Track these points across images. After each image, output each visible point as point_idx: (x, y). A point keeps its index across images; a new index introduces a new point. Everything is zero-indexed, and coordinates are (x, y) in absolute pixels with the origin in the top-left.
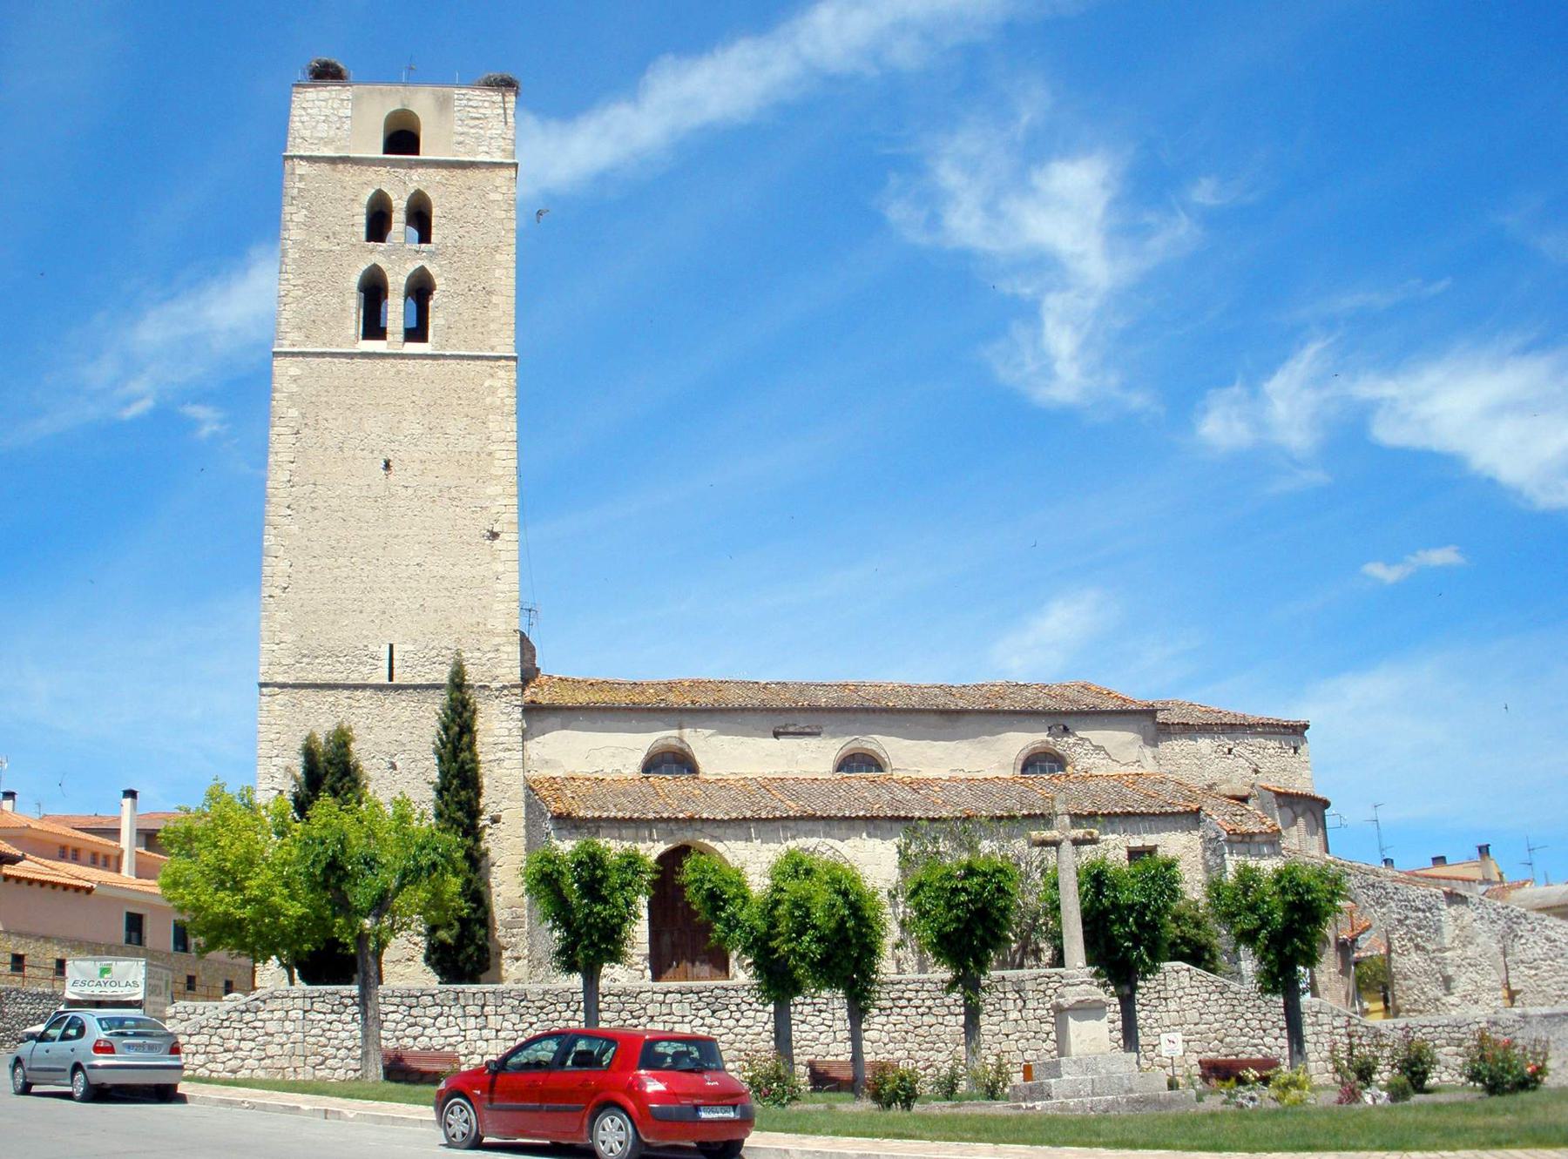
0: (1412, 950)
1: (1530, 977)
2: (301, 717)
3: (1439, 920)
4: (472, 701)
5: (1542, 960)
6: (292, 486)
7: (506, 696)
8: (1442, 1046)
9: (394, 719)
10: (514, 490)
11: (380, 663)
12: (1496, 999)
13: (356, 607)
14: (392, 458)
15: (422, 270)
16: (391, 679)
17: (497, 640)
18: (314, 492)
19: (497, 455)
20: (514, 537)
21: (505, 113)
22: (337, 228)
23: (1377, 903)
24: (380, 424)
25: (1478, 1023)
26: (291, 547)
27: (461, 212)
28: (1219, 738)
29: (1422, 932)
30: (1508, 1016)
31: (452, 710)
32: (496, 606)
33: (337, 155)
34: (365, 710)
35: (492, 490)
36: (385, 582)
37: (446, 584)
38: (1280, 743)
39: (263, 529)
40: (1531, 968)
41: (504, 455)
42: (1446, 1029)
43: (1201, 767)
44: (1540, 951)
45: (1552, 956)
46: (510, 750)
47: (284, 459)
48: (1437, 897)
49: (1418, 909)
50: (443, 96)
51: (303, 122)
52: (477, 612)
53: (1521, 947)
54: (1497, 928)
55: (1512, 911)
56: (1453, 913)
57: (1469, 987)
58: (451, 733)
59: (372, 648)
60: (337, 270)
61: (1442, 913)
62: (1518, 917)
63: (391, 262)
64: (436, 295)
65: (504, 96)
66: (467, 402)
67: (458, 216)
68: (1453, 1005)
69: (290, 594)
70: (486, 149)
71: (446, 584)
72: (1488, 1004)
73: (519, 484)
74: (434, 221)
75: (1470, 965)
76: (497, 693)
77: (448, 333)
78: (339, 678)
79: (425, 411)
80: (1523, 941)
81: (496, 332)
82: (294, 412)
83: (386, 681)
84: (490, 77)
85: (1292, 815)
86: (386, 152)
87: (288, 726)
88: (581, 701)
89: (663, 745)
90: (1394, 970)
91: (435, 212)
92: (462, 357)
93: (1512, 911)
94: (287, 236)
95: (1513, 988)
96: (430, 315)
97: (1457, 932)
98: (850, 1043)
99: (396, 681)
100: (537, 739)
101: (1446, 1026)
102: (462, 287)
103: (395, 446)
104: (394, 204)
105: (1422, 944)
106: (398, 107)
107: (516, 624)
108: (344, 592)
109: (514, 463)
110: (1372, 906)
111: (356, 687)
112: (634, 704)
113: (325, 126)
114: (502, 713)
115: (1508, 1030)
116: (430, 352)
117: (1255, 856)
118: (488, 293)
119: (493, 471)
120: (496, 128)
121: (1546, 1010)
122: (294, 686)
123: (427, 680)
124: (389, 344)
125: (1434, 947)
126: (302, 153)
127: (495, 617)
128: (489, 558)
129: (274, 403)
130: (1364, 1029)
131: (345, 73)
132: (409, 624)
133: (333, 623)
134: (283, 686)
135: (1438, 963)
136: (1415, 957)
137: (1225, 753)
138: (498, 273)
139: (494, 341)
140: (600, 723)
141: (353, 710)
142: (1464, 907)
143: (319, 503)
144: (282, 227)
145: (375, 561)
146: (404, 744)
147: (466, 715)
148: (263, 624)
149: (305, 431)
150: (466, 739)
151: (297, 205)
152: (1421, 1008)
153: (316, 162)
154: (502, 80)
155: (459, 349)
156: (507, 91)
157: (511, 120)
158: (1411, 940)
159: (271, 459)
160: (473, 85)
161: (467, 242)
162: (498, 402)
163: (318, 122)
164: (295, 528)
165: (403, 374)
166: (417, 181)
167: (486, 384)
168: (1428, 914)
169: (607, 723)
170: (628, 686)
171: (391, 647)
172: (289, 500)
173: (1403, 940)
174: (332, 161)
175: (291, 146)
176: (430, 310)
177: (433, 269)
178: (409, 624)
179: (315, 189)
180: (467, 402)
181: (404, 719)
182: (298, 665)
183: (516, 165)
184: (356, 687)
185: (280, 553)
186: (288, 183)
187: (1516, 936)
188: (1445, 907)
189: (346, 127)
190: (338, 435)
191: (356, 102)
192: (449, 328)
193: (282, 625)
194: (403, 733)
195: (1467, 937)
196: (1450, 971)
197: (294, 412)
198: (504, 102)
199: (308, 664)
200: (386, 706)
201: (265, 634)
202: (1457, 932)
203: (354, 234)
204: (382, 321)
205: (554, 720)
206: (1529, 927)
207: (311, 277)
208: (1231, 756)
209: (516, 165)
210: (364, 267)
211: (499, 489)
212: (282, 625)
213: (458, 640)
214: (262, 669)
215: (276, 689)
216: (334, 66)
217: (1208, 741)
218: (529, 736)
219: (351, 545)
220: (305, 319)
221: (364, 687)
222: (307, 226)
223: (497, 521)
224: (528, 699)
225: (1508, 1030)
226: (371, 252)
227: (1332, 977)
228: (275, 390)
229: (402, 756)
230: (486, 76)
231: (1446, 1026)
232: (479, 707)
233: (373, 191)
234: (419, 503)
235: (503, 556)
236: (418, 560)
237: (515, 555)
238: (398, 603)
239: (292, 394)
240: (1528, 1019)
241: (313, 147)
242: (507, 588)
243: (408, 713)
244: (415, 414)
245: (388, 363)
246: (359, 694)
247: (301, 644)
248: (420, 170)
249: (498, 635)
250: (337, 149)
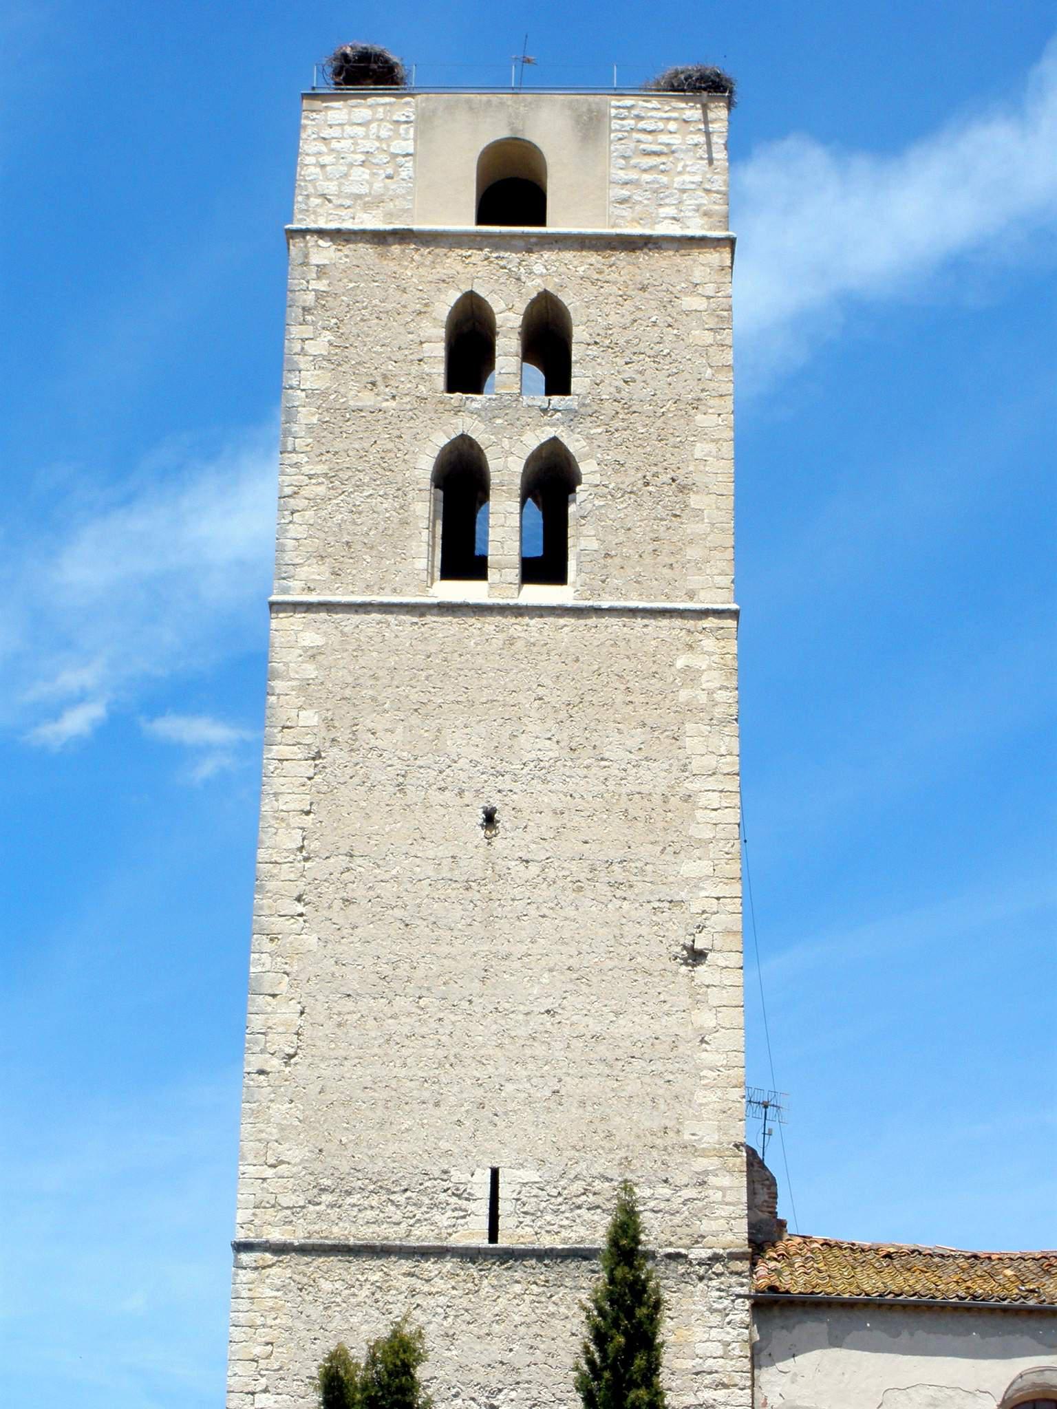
2: (315, 1312)
4: (652, 1284)
6: (306, 859)
7: (719, 1275)
9: (499, 1318)
10: (735, 868)
11: (471, 1206)
13: (426, 1095)
14: (498, 805)
15: (555, 441)
16: (493, 1237)
17: (701, 1164)
18: (348, 870)
19: (703, 800)
20: (736, 959)
21: (709, 143)
22: (390, 366)
24: (475, 740)
26: (303, 976)
27: (629, 334)
31: (613, 1302)
32: (701, 1096)
33: (389, 227)
34: (442, 1300)
35: (691, 868)
36: (484, 1046)
37: (602, 1050)
39: (249, 942)
41: (714, 800)
46: (725, 1386)
47: (291, 806)
50: (590, 111)
51: (323, 166)
52: (663, 1107)
58: (610, 1348)
59: (456, 1176)
60: (390, 446)
63: (496, 431)
64: (582, 492)
65: (705, 108)
66: (642, 699)
67: (622, 342)
69: (300, 1068)
70: (671, 211)
71: (602, 1050)
73: (744, 857)
74: (576, 352)
76: (702, 1271)
77: (605, 566)
78: (393, 1235)
79: (563, 715)
81: (699, 566)
82: (310, 718)
83: (484, 1243)
84: (676, 74)
86: (481, 220)
87: (289, 1329)
88: (867, 1288)
89: (1034, 1385)
91: (579, 334)
92: (633, 612)
94: (294, 383)
96: (570, 531)
98: (733, 497)
99: (503, 1242)
100: (781, 1365)
102: (631, 478)
103: (505, 783)
104: (499, 319)
106: (504, 133)
107: (739, 1133)
108: (405, 1065)
109: (734, 816)
111: (424, 1253)
112: (974, 1298)
113: (364, 173)
114: (712, 1311)
116: (570, 603)
118: (683, 489)
119: (693, 831)
120: (692, 170)
122: (303, 1250)
123: (564, 1241)
124: (491, 587)
126: (322, 224)
127: (699, 1118)
128: (685, 1001)
129: (273, 699)
131: (401, 72)
132: (531, 1129)
133: (382, 1124)
134: (281, 1249)
138: (700, 450)
139: (694, 581)
140: (905, 1335)
141: (418, 1300)
143: (357, 891)
144: (286, 367)
145: (465, 1004)
146: (516, 1370)
147: (641, 1312)
148: (246, 1129)
149: (332, 754)
150: (640, 1362)
151: (313, 323)
153: (348, 241)
154: (702, 78)
155: (625, 596)
156: (713, 99)
157: (720, 155)
159: (267, 806)
160: (645, 91)
161: (639, 391)
162: (703, 698)
163: (351, 165)
164: (311, 940)
165: (520, 644)
166: (541, 275)
167: (680, 663)
169: (920, 1335)
170: (961, 1262)
171: (495, 1173)
172: (301, 886)
174: (379, 238)
175: (302, 211)
176: (571, 522)
177: (574, 445)
178: (531, 1129)
179: (348, 292)
180: (642, 699)
181: (517, 1319)
182: (311, 1208)
183: (731, 242)
184: (424, 1253)
185: (283, 987)
186: (295, 282)
189: (404, 174)
190: (395, 761)
191: (423, 123)
192: (607, 555)
193: (282, 1129)
194: (516, 1347)
197: (310, 718)
198: (706, 122)
199: (332, 1206)
200: (483, 1293)
201: (249, 1146)
203: (424, 378)
204: (478, 545)
205: (813, 1326)
207: (345, 461)
209: (731, 242)
210: (442, 440)
211: (704, 867)
212: (282, 1129)
213: (626, 1162)
214: (242, 1216)
215: (268, 1256)
216: (379, 57)
218: (763, 1357)
219: (420, 973)
220: (331, 539)
221: (440, 1253)
222: (332, 362)
223: (701, 928)
224: (763, 1283)
226: (457, 411)
228: (275, 675)
229: (513, 1395)
230: (670, 70)
232: (666, 1296)
233: (459, 295)
234: (550, 893)
235: (714, 997)
236: (548, 1004)
237: (737, 996)
238: (509, 1087)
239: (307, 683)
241: (343, 212)
242: (720, 1060)
243: (525, 1308)
244: (543, 720)
245: (491, 623)
246: (430, 1267)
247: (318, 1166)
248: (547, 255)
249: (704, 1153)
250: (389, 215)
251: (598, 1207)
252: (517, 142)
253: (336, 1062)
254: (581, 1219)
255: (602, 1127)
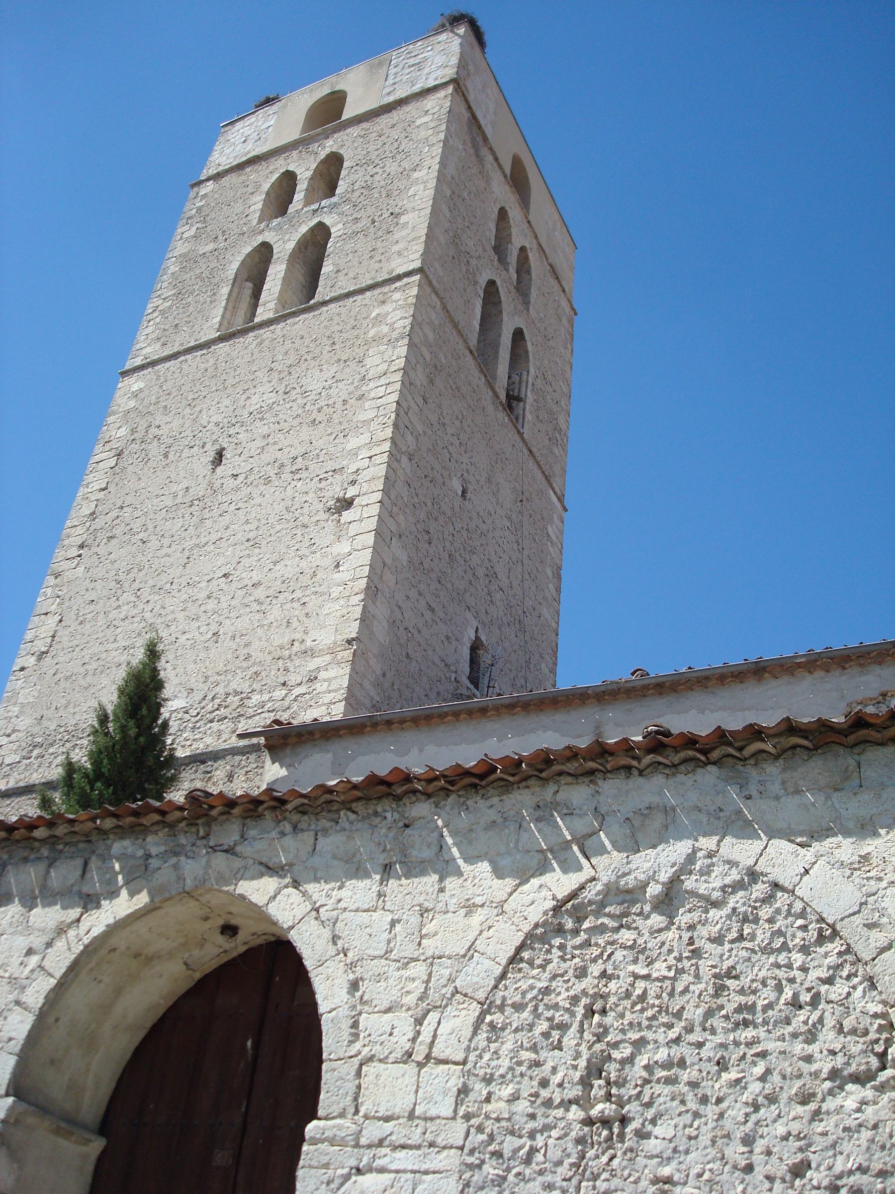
47: (95, 489)
251: (226, 718)
252: (335, 96)
253: (71, 650)
254: (698, 1029)
255: (243, 652)
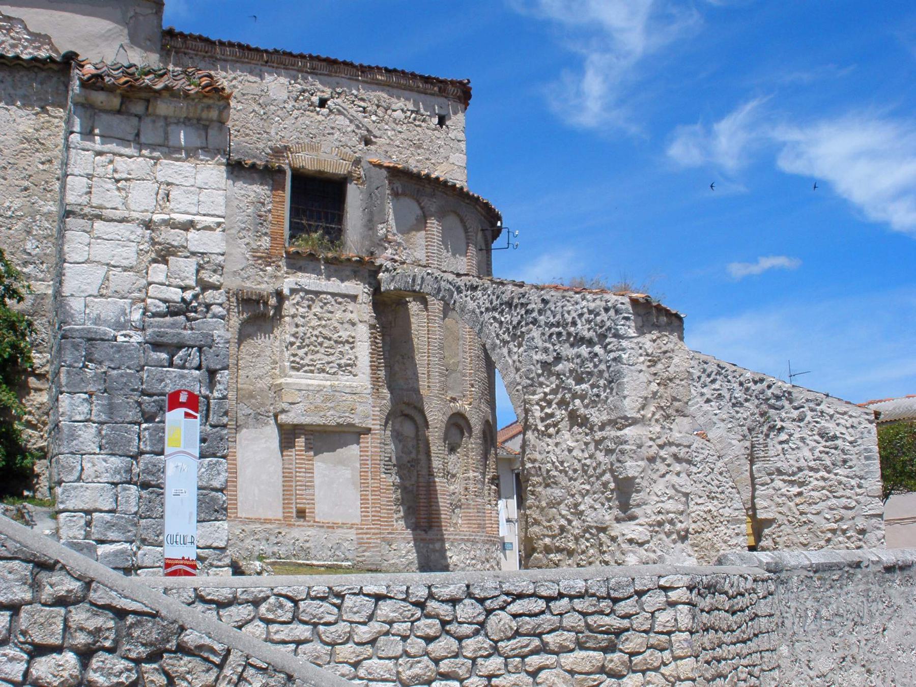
0: (565, 424)
1: (790, 498)
3: (617, 360)
5: (811, 469)
8: (564, 650)
12: (737, 534)
23: (514, 337)
25: (665, 589)
28: (304, 79)
29: (584, 386)
30: (744, 569)
38: (416, 104)
40: (792, 483)
42: (578, 604)
43: (266, 117)
44: (808, 454)
45: (829, 463)
48: (617, 312)
49: (580, 341)
53: (780, 447)
54: (743, 413)
55: (769, 387)
56: (649, 346)
57: (670, 505)
61: (624, 343)
62: (778, 398)
68: (631, 541)
72: (725, 542)
75: (676, 457)
80: (783, 437)
85: (419, 212)
90: (529, 465)
93: (769, 387)
95: (761, 515)
97: (654, 387)
101: (581, 596)
105: (582, 411)
110: (506, 343)
115: (741, 602)
117: (153, 147)
121: (816, 557)
125: (605, 417)
130: (106, 622)
135: (609, 452)
136: (567, 438)
137: (312, 104)
142: (674, 338)
152: (572, 545)
158: (563, 403)
168: (597, 349)
173: (549, 403)
187: (772, 428)
188: (632, 332)
195: (675, 399)
196: (632, 468)
202: (654, 387)
206: (795, 414)
208: (325, 111)
217: (282, 80)
225: (741, 602)
227: (472, 488)
231: (581, 596)
240: (783, 575)
